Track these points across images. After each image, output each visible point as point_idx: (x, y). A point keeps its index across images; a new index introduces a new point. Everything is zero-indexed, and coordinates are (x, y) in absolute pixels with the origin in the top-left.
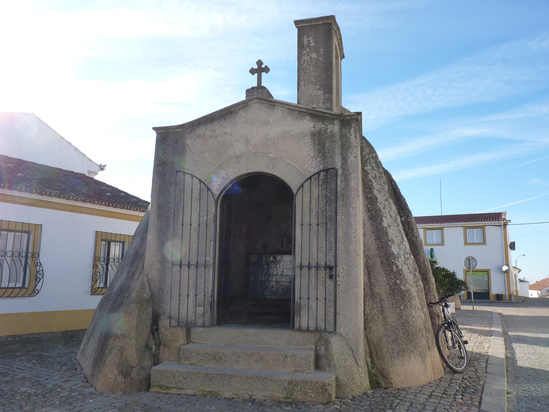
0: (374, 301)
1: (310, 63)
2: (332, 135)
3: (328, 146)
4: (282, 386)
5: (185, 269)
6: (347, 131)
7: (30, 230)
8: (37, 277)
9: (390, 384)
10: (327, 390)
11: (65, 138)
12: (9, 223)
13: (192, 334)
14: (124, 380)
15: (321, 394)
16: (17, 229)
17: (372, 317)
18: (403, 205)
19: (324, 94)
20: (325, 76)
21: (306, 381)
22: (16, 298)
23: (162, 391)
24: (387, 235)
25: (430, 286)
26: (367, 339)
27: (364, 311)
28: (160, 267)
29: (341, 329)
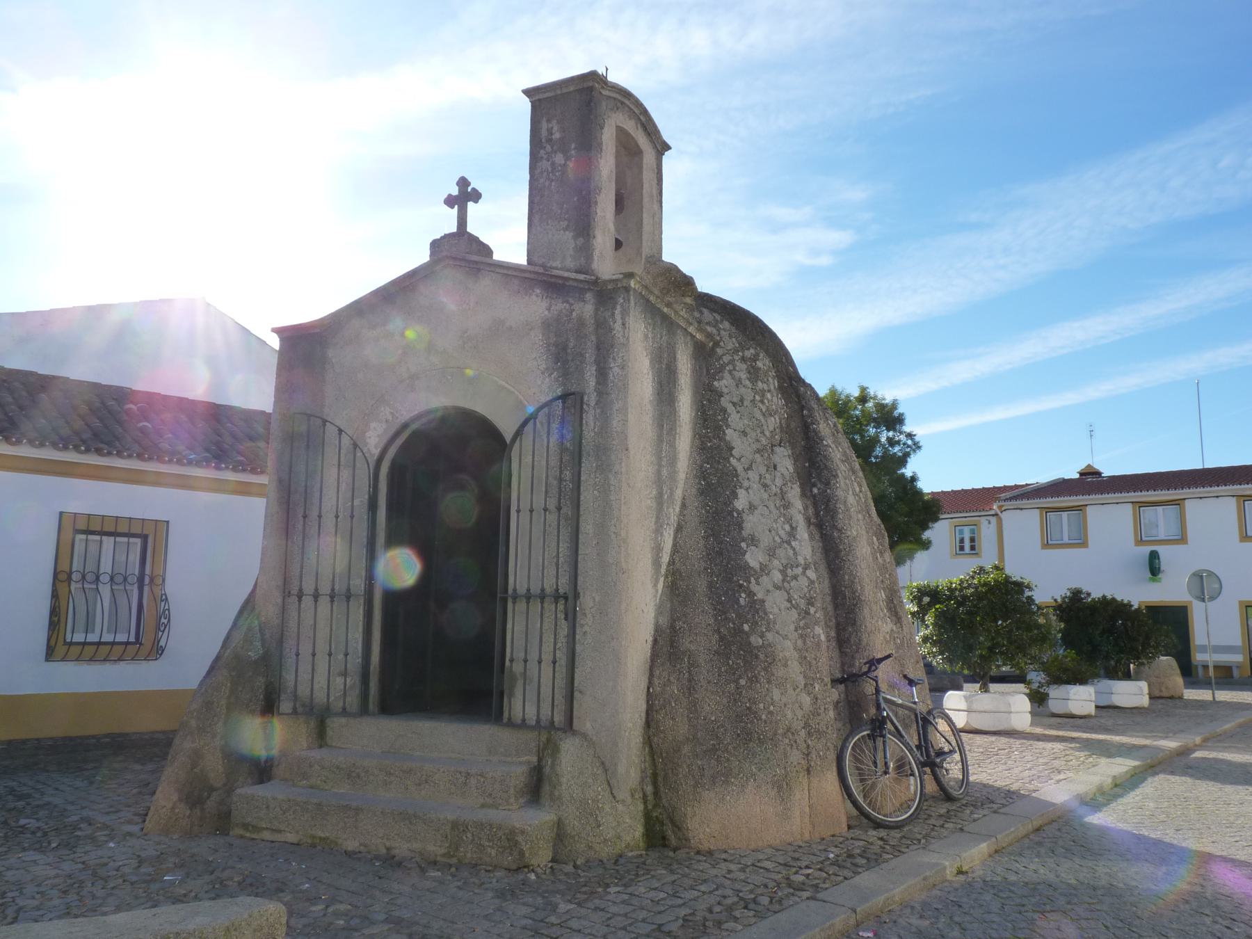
0: (675, 667)
1: (551, 175)
2: (581, 323)
4: (441, 832)
5: (324, 603)
6: (608, 314)
7: (145, 532)
8: (162, 622)
9: (686, 840)
10: (517, 843)
11: (268, 343)
12: (103, 519)
13: (328, 729)
14: (188, 812)
15: (507, 851)
16: (133, 531)
17: (664, 701)
18: (821, 460)
19: (575, 238)
21: (482, 825)
22: (121, 663)
23: (248, 835)
24: (741, 528)
25: (860, 637)
26: (651, 747)
27: (648, 688)
29: (584, 723)
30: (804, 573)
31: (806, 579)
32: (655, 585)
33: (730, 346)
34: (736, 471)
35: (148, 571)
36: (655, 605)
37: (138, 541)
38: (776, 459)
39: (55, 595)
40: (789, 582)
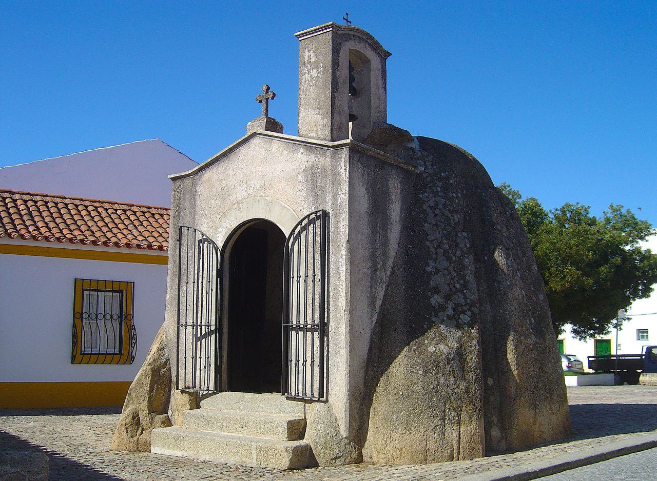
37: (118, 294)
39: (74, 326)
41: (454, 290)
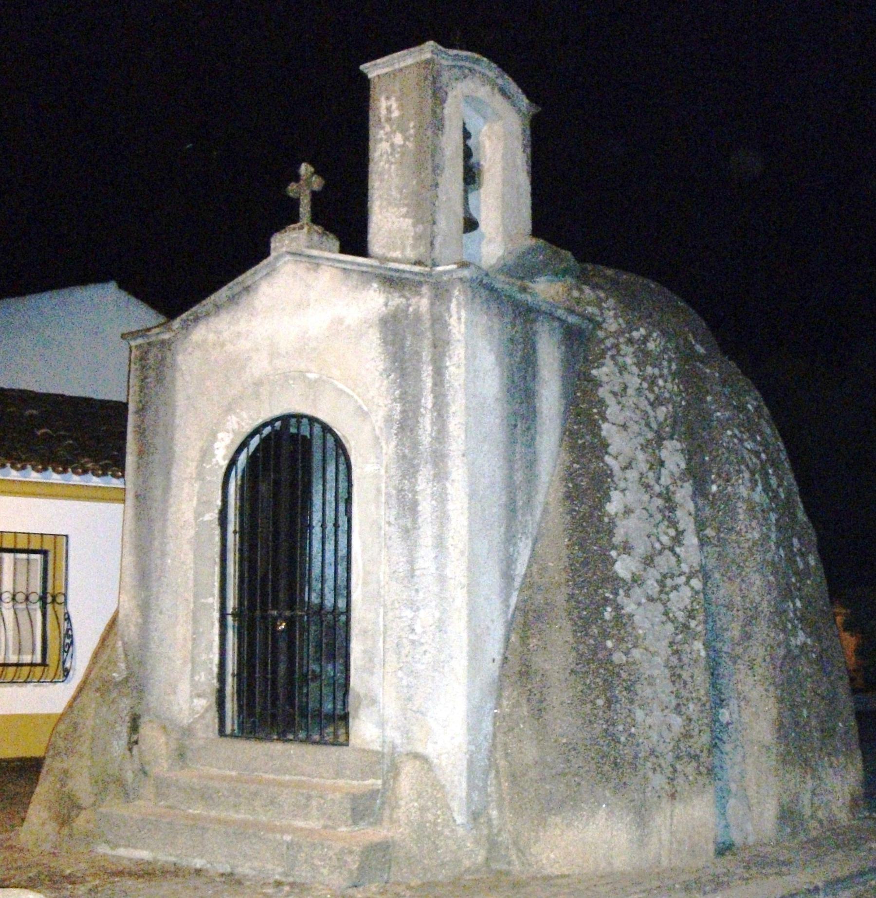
2: (418, 317)
3: (411, 346)
16: (19, 546)
20: (417, 183)
24: (611, 533)
28: (140, 621)
30: (687, 583)
31: (689, 589)
32: (506, 600)
33: (613, 327)
34: (611, 470)
35: (50, 589)
36: (506, 622)
37: (38, 557)
38: (664, 454)
40: (667, 594)
41: (658, 546)
